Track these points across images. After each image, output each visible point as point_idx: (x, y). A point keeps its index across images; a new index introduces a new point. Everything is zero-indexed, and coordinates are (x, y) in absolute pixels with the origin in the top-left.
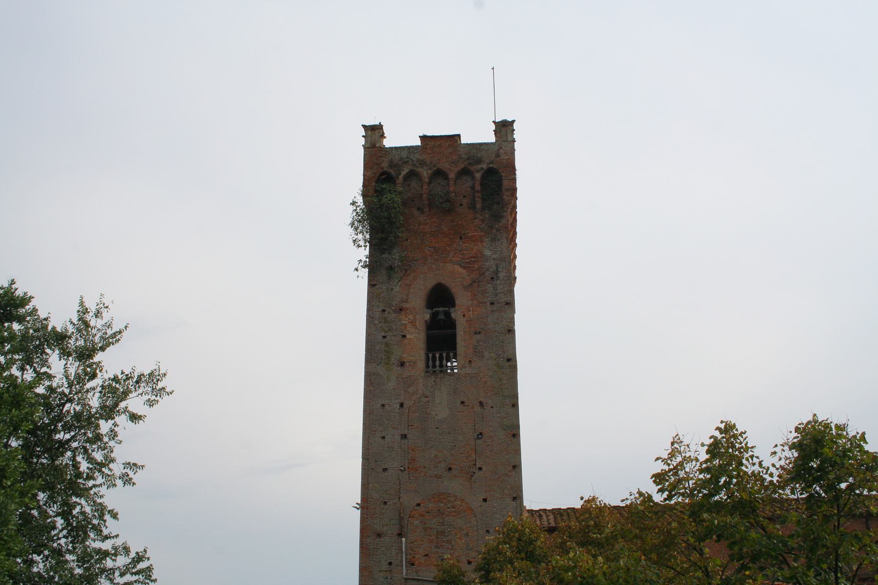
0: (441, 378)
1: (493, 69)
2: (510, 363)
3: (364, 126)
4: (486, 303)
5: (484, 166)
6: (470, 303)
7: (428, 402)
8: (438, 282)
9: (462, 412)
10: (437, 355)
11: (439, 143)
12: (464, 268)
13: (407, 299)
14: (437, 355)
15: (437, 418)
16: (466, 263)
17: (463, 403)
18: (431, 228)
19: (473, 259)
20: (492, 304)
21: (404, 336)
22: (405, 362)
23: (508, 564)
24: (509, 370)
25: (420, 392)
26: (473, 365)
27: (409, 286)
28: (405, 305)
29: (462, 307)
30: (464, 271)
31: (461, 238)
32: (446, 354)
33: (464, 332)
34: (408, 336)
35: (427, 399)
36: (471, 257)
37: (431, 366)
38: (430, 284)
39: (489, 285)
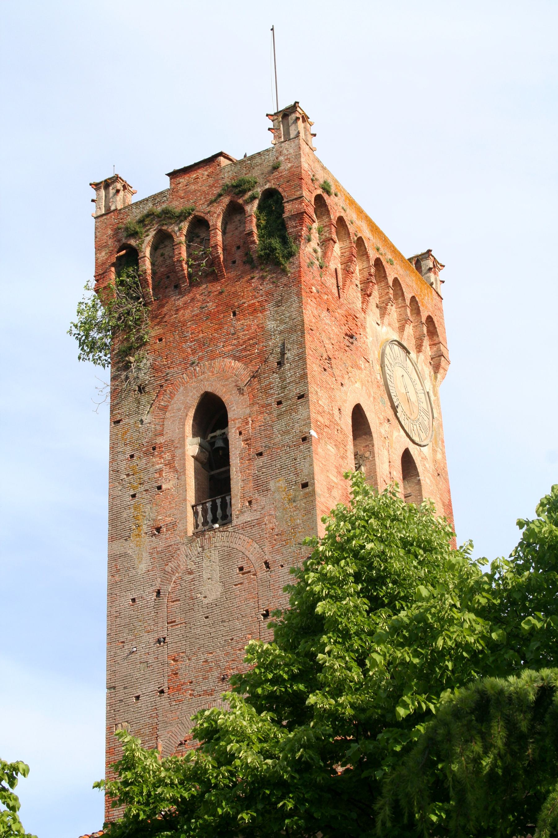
0: (210, 538)
1: (272, 29)
2: (307, 490)
3: (169, 175)
4: (269, 405)
5: (259, 190)
6: (248, 411)
7: (193, 580)
8: (202, 392)
9: (241, 584)
10: (219, 502)
11: (195, 176)
12: (238, 359)
13: (163, 430)
14: (219, 502)
15: (206, 601)
16: (241, 350)
17: (241, 569)
18: (192, 311)
19: (251, 342)
20: (279, 403)
21: (159, 488)
22: (161, 527)
23: (252, 818)
24: (305, 501)
25: (182, 567)
26: (254, 506)
27: (164, 409)
28: (160, 440)
29: (237, 421)
30: (238, 364)
31: (234, 314)
32: (220, 500)
33: (242, 459)
34: (164, 487)
35: (192, 576)
36: (249, 339)
37: (219, 519)
38: (193, 400)
39: (275, 375)
